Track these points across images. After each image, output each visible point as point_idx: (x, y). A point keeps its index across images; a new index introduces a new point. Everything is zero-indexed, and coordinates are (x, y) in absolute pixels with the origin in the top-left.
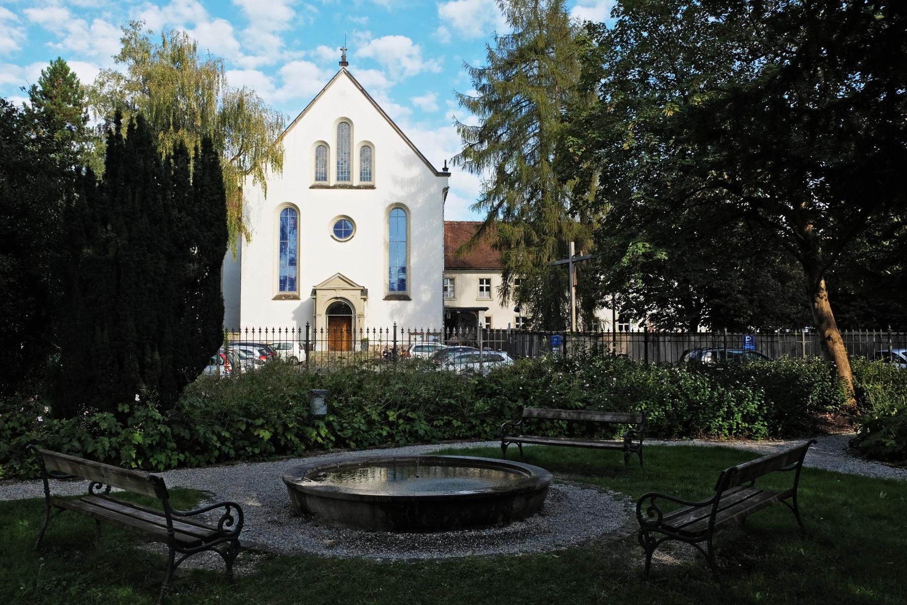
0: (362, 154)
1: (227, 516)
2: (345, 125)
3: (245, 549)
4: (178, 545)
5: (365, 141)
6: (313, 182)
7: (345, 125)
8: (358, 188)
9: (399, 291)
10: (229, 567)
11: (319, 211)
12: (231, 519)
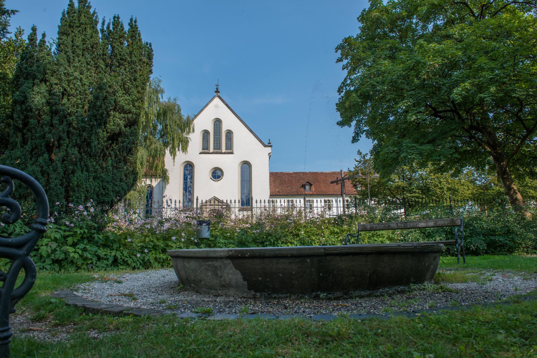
0: (227, 136)
2: (218, 122)
5: (228, 130)
6: (201, 151)
7: (218, 122)
11: (204, 164)
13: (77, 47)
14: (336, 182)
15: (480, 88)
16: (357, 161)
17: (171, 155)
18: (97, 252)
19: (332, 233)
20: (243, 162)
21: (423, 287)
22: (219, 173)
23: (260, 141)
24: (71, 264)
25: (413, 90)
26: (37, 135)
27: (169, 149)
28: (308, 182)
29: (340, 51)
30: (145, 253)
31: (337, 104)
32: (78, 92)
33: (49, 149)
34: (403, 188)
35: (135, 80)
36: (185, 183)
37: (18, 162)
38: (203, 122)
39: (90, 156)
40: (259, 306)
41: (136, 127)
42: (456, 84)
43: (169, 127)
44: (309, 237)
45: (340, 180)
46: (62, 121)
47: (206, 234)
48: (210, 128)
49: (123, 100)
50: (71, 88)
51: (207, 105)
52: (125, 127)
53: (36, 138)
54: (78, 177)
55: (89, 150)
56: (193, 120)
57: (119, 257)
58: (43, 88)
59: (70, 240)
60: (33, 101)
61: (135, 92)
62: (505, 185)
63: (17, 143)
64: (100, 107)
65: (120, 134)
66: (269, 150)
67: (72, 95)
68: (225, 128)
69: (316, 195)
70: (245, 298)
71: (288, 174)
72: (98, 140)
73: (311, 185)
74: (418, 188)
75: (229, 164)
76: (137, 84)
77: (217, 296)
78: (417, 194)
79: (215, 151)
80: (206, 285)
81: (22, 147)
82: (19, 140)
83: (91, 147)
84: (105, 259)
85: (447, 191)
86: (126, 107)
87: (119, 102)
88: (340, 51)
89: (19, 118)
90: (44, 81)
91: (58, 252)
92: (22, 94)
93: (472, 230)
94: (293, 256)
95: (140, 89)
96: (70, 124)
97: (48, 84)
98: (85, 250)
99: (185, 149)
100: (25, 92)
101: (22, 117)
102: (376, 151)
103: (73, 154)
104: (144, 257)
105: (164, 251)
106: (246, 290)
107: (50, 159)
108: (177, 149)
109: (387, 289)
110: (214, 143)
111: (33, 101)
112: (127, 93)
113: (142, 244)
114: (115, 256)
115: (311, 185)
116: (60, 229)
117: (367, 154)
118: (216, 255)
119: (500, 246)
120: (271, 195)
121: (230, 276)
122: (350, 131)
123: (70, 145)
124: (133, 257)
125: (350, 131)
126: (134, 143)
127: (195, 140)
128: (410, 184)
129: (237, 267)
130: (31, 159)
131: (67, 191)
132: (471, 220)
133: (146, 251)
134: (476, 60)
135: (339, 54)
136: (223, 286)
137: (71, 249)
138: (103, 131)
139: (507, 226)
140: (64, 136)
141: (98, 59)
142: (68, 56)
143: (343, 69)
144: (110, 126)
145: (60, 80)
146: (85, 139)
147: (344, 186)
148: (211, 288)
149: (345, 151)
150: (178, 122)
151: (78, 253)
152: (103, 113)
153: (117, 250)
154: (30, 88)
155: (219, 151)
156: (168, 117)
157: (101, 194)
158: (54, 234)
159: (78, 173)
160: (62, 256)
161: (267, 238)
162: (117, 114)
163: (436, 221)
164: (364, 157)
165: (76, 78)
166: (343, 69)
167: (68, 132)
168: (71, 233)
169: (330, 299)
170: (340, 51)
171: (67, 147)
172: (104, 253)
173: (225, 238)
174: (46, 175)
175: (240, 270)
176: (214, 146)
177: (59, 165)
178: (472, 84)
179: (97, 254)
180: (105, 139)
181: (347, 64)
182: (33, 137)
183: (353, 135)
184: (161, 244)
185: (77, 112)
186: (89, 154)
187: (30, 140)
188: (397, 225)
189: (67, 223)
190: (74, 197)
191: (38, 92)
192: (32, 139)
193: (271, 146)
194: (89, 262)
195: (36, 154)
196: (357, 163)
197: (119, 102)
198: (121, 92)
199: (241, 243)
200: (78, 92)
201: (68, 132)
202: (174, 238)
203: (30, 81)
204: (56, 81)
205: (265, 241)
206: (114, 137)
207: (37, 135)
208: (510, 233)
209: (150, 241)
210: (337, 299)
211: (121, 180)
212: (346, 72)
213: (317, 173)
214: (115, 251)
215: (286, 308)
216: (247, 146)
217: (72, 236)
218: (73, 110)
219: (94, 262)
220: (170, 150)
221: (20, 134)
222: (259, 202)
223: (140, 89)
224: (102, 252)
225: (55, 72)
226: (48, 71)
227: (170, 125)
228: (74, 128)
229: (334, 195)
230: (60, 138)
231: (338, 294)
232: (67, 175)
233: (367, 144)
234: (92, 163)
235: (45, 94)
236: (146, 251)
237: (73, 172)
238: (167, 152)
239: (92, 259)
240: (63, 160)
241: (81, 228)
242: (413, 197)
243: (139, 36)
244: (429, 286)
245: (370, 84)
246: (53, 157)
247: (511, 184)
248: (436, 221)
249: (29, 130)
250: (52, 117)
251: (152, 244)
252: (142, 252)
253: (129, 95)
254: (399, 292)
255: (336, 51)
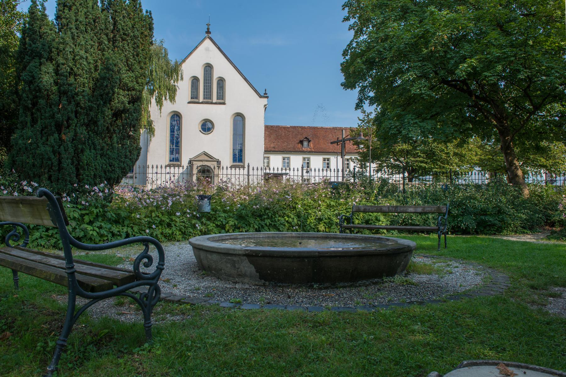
0: (218, 84)
1: (145, 255)
2: (208, 68)
3: (414, 249)
4: (78, 287)
5: (220, 77)
6: (190, 100)
7: (208, 68)
8: (216, 103)
9: (238, 157)
10: (147, 318)
11: (193, 115)
12: (150, 259)
13: (81, 22)
14: (337, 142)
15: (489, 65)
16: (361, 120)
17: (157, 105)
18: (111, 229)
19: (329, 206)
20: (235, 114)
21: (393, 279)
22: (209, 125)
23: (256, 91)
24: (89, 241)
25: (420, 61)
26: (47, 115)
27: (154, 97)
28: (306, 138)
29: (347, 9)
30: (153, 228)
31: (341, 64)
32: (84, 71)
33: (59, 127)
34: (407, 151)
35: (138, 55)
36: (172, 136)
37: (30, 142)
38: (192, 67)
39: (97, 134)
40: (269, 295)
41: (139, 104)
42: (463, 59)
43: (154, 73)
44: (305, 209)
45: (341, 141)
46: (70, 101)
47: (207, 208)
48: (200, 75)
49: (126, 77)
50: (78, 68)
51: (197, 47)
52: (129, 104)
53: (46, 118)
54: (87, 156)
55: (96, 128)
56: (181, 64)
57: (131, 233)
58: (50, 67)
59: (87, 219)
60: (41, 81)
61: (138, 68)
62: (507, 160)
63: (27, 123)
64: (104, 87)
65: (125, 111)
66: (265, 101)
67: (79, 75)
68: (216, 75)
69: (315, 152)
70: (257, 285)
71: (285, 128)
72: (104, 118)
73: (309, 141)
74: (423, 152)
75: (221, 115)
76: (140, 60)
77: (236, 283)
78: (421, 159)
79: (205, 100)
80: (226, 274)
81: (32, 126)
82: (29, 119)
83: (97, 126)
84: (119, 236)
85: (453, 156)
86: (130, 85)
87: (123, 79)
88: (347, 9)
89: (28, 97)
90: (50, 59)
91: (78, 230)
92: (30, 74)
93: (465, 209)
94: (294, 257)
95: (142, 65)
96: (78, 104)
97: (54, 62)
98: (100, 227)
99: (172, 99)
100: (32, 72)
101: (31, 97)
102: (378, 120)
103: (82, 134)
104: (153, 233)
105: (169, 225)
106: (258, 279)
107: (60, 139)
108: (164, 98)
109: (364, 281)
110: (204, 92)
111: (41, 81)
112: (130, 69)
113: (148, 219)
114: (127, 232)
115: (309, 141)
116: (77, 208)
117: (371, 113)
118: (235, 253)
119: (489, 226)
120: (265, 151)
121: (246, 268)
122: (355, 93)
123: (78, 125)
124: (143, 232)
125: (355, 93)
126: (137, 120)
127: (183, 88)
128: (415, 148)
129: (251, 262)
130: (41, 139)
131: (77, 170)
132: (464, 199)
133: (154, 226)
134: (489, 33)
135: (346, 12)
136: (239, 275)
137: (89, 228)
138: (108, 109)
139: (498, 207)
140: (73, 116)
141: (100, 34)
142: (72, 33)
143: (349, 30)
144: (116, 104)
145: (66, 59)
146: (92, 118)
147: (345, 147)
148: (229, 276)
149: (348, 111)
150: (165, 68)
151: (96, 231)
152: (109, 93)
153: (128, 226)
154: (37, 68)
155: (209, 100)
156: (154, 62)
157: (108, 171)
158: (72, 213)
159: (87, 152)
160: (82, 234)
161: (265, 211)
162: (121, 92)
163: (424, 208)
164: (368, 116)
165: (82, 58)
166: (349, 30)
167: (76, 112)
168: (87, 212)
169: (320, 289)
170: (347, 9)
171: (76, 126)
172: (117, 230)
173: (225, 211)
174: (57, 154)
175: (254, 265)
176: (204, 95)
177: (70, 145)
178: (480, 61)
179: (111, 230)
180: (110, 117)
181: (354, 24)
182: (43, 117)
183: (357, 102)
184: (166, 219)
185: (84, 91)
186: (96, 132)
187: (39, 120)
188: (389, 209)
189: (83, 203)
190: (84, 175)
191: (45, 72)
192: (41, 119)
193: (267, 97)
194: (105, 238)
195: (46, 133)
196: (360, 122)
197: (123, 79)
198: (124, 69)
199: (240, 217)
200: (84, 71)
201: (76, 112)
202: (178, 214)
203: (37, 60)
204: (64, 61)
205: (263, 215)
206: (117, 114)
207: (47, 115)
208: (501, 213)
209: (156, 216)
210: (326, 288)
211: (126, 157)
212: (352, 32)
213: (317, 128)
214: (126, 227)
215: (289, 297)
216: (240, 95)
217: (87, 214)
218: (80, 89)
219: (110, 238)
220: (156, 99)
221: (29, 114)
222: (255, 169)
223: (142, 65)
224: (115, 229)
225: (61, 51)
226: (53, 50)
227: (156, 71)
228: (81, 108)
229: (334, 152)
230: (69, 118)
231: (327, 284)
232: (78, 153)
233: (372, 110)
234: (98, 141)
235: (53, 74)
236: (154, 226)
237: (82, 151)
238: (153, 101)
239: (107, 236)
240: (73, 140)
241: (96, 208)
242: (416, 161)
243: (140, 7)
244: (398, 278)
245: (377, 50)
246: (64, 137)
247: (514, 159)
248: (424, 208)
249: (38, 110)
250: (60, 97)
251: (159, 220)
252: (150, 228)
253: (133, 71)
254: (374, 283)
255: (343, 9)
